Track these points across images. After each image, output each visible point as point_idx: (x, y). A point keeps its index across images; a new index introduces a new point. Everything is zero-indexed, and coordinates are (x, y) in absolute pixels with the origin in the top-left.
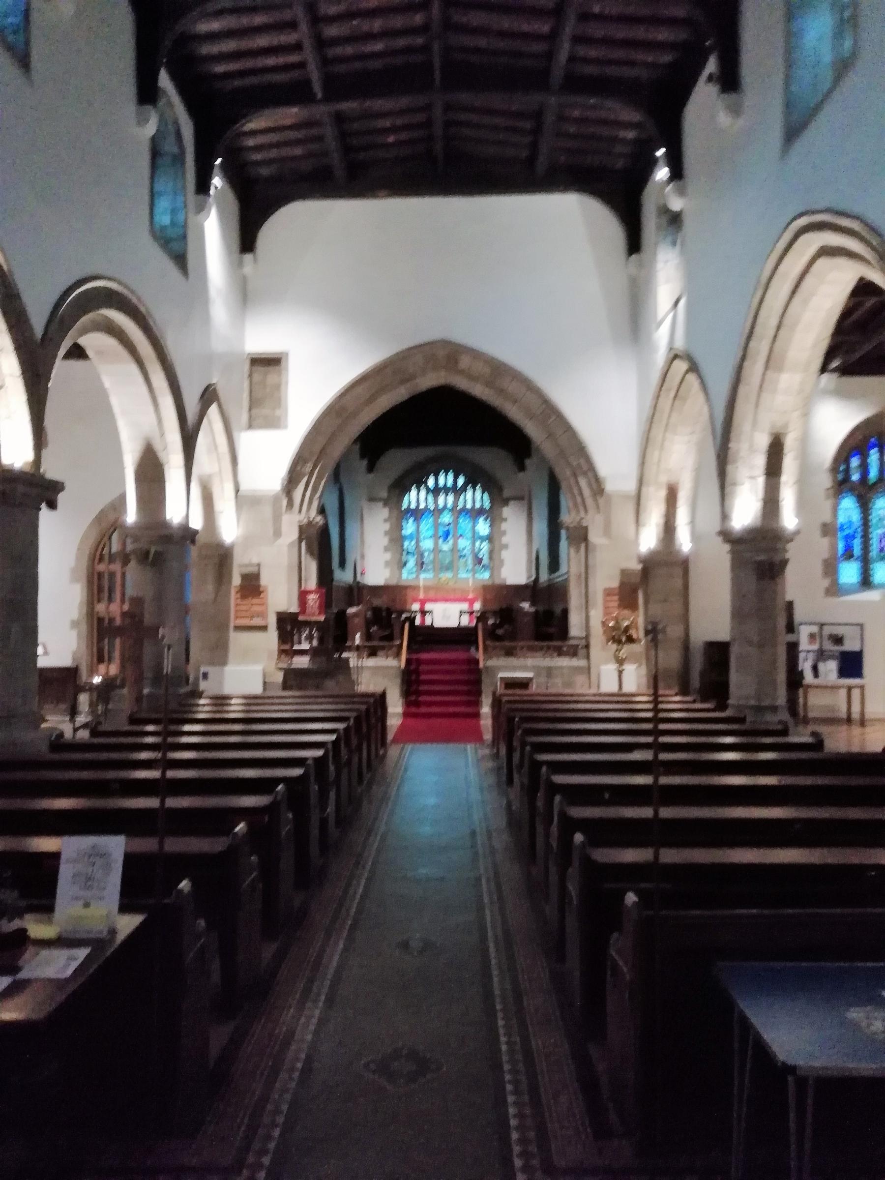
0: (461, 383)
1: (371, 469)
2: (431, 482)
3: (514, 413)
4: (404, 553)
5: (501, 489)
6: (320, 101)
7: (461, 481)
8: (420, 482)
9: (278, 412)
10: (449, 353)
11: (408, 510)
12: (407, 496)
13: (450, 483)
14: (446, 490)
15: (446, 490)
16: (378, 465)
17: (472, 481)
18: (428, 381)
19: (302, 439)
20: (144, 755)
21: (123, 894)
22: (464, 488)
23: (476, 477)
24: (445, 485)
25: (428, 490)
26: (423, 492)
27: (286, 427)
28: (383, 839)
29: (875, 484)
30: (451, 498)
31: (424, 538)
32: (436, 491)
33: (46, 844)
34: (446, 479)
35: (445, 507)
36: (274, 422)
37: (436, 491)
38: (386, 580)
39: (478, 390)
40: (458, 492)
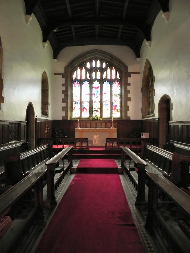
2: (88, 65)
4: (74, 103)
7: (104, 65)
8: (82, 65)
11: (76, 80)
12: (75, 73)
13: (98, 66)
14: (96, 69)
15: (96, 69)
16: (59, 56)
17: (110, 65)
20: (96, 99)
21: (131, 99)
22: (106, 69)
23: (112, 62)
25: (87, 70)
26: (84, 70)
28: (188, 92)
30: (99, 73)
31: (98, 88)
32: (90, 71)
34: (96, 64)
37: (90, 71)
38: (63, 117)
40: (102, 71)
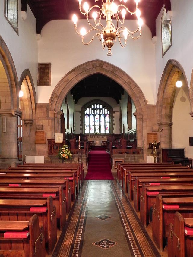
0: (104, 73)
1: (76, 103)
2: (93, 107)
3: (119, 81)
5: (112, 108)
6: (79, 135)
9: (48, 81)
10: (100, 64)
12: (86, 110)
13: (98, 107)
14: (97, 109)
15: (97, 109)
17: (104, 107)
18: (94, 71)
19: (36, 24)
24: (97, 110)
25: (92, 109)
27: (51, 85)
29: (35, 214)
32: (94, 110)
33: (163, 163)
35: (97, 114)
36: (47, 84)
39: (109, 75)
40: (100, 110)
